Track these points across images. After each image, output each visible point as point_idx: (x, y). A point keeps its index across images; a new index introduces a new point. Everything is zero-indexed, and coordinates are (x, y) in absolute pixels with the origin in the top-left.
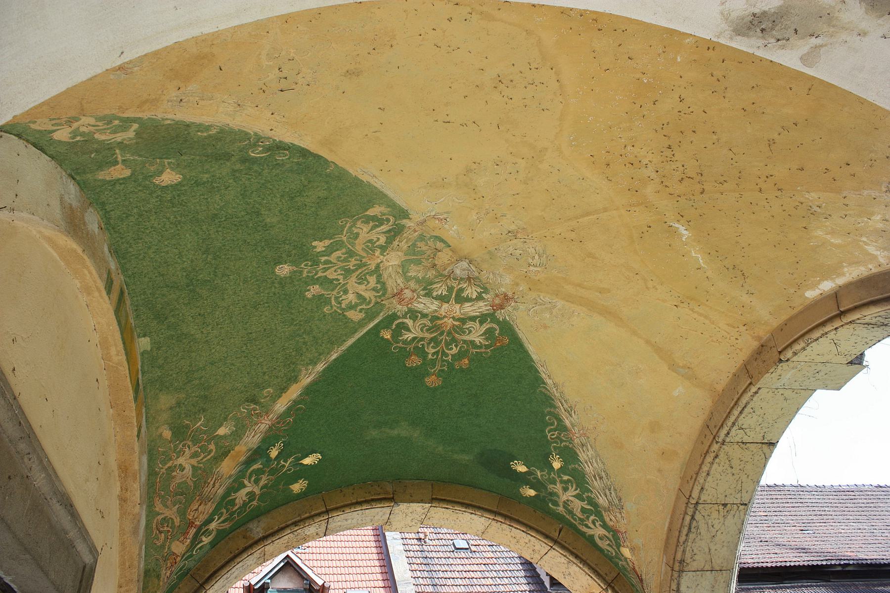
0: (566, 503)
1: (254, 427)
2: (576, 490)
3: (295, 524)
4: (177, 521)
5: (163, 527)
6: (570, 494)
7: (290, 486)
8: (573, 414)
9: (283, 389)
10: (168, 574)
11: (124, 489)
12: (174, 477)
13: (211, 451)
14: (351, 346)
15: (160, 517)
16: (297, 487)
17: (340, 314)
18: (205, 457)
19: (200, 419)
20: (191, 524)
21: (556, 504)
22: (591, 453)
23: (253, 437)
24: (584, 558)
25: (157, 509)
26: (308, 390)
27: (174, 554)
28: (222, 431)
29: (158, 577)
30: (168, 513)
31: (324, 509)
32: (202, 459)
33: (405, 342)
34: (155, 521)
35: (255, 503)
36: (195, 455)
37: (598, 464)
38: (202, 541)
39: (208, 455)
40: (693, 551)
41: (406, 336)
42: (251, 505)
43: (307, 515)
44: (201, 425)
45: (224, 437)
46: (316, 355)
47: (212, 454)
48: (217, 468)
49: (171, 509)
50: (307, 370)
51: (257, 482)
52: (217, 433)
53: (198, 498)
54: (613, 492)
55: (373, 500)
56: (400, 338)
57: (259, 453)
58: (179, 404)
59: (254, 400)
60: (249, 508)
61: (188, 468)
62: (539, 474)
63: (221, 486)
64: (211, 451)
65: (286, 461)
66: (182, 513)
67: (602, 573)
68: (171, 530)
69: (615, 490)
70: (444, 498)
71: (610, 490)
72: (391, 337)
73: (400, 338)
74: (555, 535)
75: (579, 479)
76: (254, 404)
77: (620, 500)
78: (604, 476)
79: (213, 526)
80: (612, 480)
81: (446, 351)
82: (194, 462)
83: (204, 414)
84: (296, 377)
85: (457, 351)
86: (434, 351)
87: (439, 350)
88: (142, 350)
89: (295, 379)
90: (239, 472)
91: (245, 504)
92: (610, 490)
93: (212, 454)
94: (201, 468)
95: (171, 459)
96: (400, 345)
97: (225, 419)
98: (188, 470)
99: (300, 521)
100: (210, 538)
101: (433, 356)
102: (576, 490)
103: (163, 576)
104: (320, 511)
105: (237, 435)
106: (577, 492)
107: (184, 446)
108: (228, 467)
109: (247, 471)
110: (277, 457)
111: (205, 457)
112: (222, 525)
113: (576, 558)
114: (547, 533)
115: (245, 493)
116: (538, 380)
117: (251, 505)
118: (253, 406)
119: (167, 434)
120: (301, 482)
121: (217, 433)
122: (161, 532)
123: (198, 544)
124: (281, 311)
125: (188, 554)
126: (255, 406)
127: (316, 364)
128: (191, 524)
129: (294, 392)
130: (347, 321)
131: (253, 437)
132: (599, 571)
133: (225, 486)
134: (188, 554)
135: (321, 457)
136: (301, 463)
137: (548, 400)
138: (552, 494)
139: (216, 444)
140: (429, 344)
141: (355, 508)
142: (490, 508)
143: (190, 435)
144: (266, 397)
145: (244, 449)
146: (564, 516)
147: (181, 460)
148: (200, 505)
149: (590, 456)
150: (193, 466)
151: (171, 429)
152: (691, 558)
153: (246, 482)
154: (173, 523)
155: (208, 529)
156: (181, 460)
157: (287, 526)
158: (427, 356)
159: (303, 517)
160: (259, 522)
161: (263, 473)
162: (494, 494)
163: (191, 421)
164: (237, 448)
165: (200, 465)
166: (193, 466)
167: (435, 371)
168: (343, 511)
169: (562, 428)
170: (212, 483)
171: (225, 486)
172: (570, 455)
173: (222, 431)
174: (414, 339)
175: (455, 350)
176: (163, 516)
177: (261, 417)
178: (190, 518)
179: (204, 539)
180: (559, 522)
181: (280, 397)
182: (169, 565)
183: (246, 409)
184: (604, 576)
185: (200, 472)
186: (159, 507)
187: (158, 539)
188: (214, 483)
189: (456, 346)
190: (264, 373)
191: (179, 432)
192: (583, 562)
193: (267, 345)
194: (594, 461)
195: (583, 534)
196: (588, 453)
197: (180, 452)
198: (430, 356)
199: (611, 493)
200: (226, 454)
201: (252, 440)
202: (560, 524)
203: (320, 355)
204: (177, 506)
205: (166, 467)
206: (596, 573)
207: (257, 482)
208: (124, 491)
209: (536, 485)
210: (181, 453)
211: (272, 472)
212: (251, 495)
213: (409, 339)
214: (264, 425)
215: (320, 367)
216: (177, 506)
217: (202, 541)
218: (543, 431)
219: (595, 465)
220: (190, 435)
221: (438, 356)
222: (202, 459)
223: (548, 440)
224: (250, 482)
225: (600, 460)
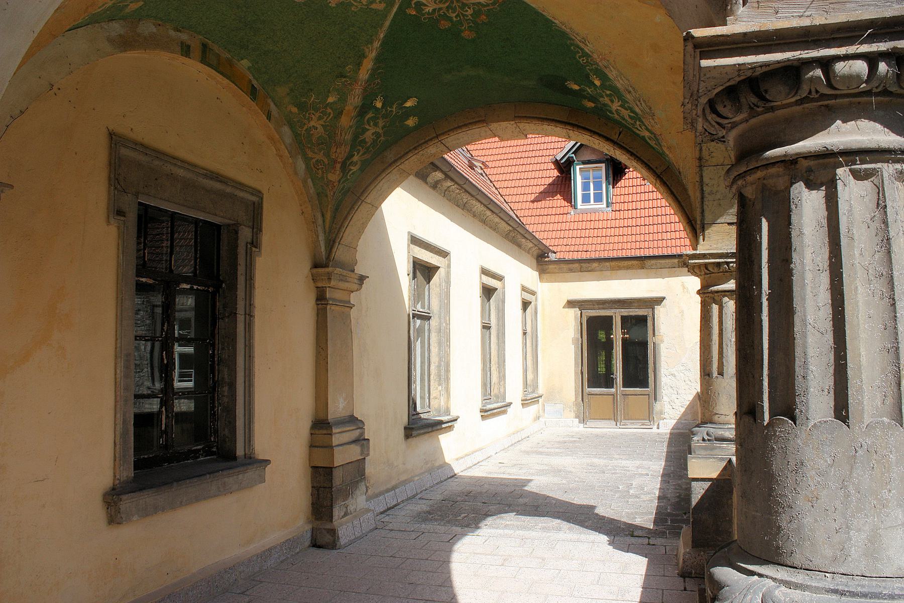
0: (617, 111)
1: (351, 93)
2: (619, 101)
3: (415, 148)
4: (326, 160)
5: (318, 166)
6: (616, 105)
7: (405, 123)
8: (588, 44)
9: (359, 64)
10: (332, 194)
11: (278, 150)
12: (312, 134)
13: (330, 114)
14: (391, 26)
15: (314, 160)
16: (411, 122)
17: (366, 9)
18: (327, 118)
19: (312, 96)
20: (335, 162)
21: (611, 112)
22: (614, 73)
23: (354, 99)
24: (639, 156)
25: (310, 156)
26: (377, 60)
27: (331, 181)
28: (331, 100)
29: (327, 196)
30: (318, 157)
31: (435, 135)
32: (327, 119)
33: (429, 13)
34: (312, 163)
35: (382, 138)
36: (320, 118)
37: (623, 81)
38: (351, 170)
39: (329, 116)
40: (709, 149)
41: (427, 10)
42: (381, 140)
43: (423, 141)
44: (314, 99)
45: (334, 103)
46: (368, 37)
47: (332, 115)
48: (339, 123)
49: (319, 154)
50: (368, 48)
51: (376, 125)
52: (328, 102)
53: (334, 145)
54: (643, 103)
55: (470, 123)
56: (424, 12)
57: (364, 108)
58: (292, 90)
59: (342, 76)
60: (379, 142)
61: (319, 127)
62: (589, 91)
63: (346, 134)
64: (330, 114)
65: (391, 107)
66: (327, 155)
67: (653, 167)
68: (324, 167)
69: (644, 101)
70: (524, 115)
71: (639, 101)
72: (417, 12)
73: (424, 12)
74: (615, 138)
75: (616, 93)
76: (344, 78)
77: (650, 108)
78: (631, 90)
79: (356, 158)
80: (639, 92)
81: (464, 13)
82: (321, 122)
83: (313, 92)
84: (364, 54)
85: (472, 12)
86: (455, 15)
87: (458, 13)
88: (247, 67)
89: (364, 56)
90: (357, 122)
91: (374, 141)
92: (639, 101)
93: (332, 115)
94: (328, 125)
95: (305, 124)
96: (426, 16)
97: (329, 92)
98: (320, 129)
99: (418, 146)
100: (358, 167)
101: (457, 18)
102: (619, 101)
103: (329, 195)
104: (432, 137)
105: (343, 99)
106: (620, 102)
107: (309, 114)
108: (345, 121)
109: (364, 120)
110: (383, 107)
111: (327, 118)
112: (363, 156)
113: (631, 155)
114: (608, 136)
115: (371, 134)
116: (548, 23)
117: (381, 140)
118: (344, 80)
119: (295, 110)
120: (412, 118)
121: (328, 102)
122: (318, 169)
123: (348, 172)
124: (321, 19)
125: (343, 179)
126: (345, 79)
127: (372, 43)
128: (335, 162)
129: (368, 65)
130: (376, 12)
131: (354, 99)
132: (651, 165)
133: (350, 133)
134: (343, 179)
135: (417, 100)
136: (405, 107)
137: (564, 35)
138: (605, 105)
139: (331, 108)
140: (448, 11)
141: (457, 131)
142: (561, 120)
143: (310, 107)
144: (350, 72)
145: (351, 108)
146: (621, 122)
147: (312, 123)
148: (337, 148)
149: (615, 76)
150: (322, 125)
151: (295, 106)
152: (709, 155)
153: (367, 127)
154: (324, 162)
155: (352, 162)
156: (312, 123)
157: (410, 151)
158: (452, 19)
159: (420, 143)
160: (391, 150)
161: (378, 118)
162: (565, 108)
163: (306, 98)
164: (346, 108)
165: (326, 124)
166: (322, 125)
167: (465, 28)
168: (449, 135)
169: (587, 55)
170: (339, 133)
171: (350, 133)
172: (603, 77)
173: (331, 100)
174: (434, 10)
175: (470, 12)
176: (316, 159)
177: (353, 85)
178: (334, 157)
179: (352, 168)
180: (620, 126)
181: (359, 69)
182: (330, 188)
183: (340, 82)
184: (655, 169)
185: (329, 128)
186: (310, 154)
187: (318, 174)
188: (341, 133)
189: (470, 8)
190: (339, 58)
191: (302, 107)
192: (637, 159)
193: (328, 41)
194: (619, 79)
195: (638, 135)
196: (612, 73)
197: (308, 118)
198: (455, 19)
199: (641, 104)
200: (341, 113)
201: (355, 100)
202: (620, 128)
203: (372, 36)
204: (322, 152)
205: (304, 129)
206: (647, 168)
207: (376, 125)
208: (278, 151)
209: (592, 99)
210: (310, 119)
211: (385, 116)
212: (377, 134)
213: (430, 11)
214: (358, 90)
215: (377, 44)
216: (322, 152)
217: (351, 170)
218: (575, 58)
219: (621, 82)
220: (310, 107)
221: (460, 17)
222: (327, 119)
223: (582, 64)
224: (370, 126)
225: (624, 77)
